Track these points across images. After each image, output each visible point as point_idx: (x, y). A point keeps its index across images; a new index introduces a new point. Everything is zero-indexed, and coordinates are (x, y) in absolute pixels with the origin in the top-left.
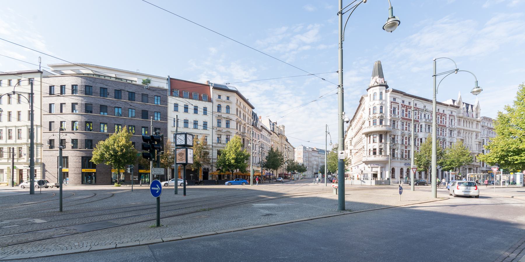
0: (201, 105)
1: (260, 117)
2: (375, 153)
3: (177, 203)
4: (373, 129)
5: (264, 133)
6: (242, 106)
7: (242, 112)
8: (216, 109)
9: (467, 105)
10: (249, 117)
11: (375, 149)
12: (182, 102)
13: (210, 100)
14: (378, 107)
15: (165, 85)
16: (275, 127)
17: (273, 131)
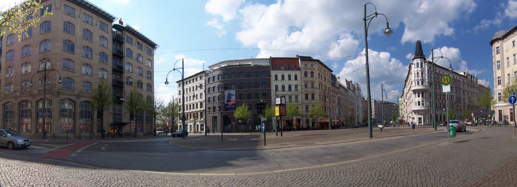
0: (293, 73)
1: (339, 78)
2: (419, 105)
3: (68, 163)
4: (417, 87)
5: (341, 90)
6: (323, 71)
7: (323, 75)
8: (303, 75)
9: (472, 76)
10: (328, 78)
11: (419, 102)
12: (279, 73)
13: (299, 69)
14: (420, 73)
15: (267, 64)
16: (351, 85)
17: (349, 88)
